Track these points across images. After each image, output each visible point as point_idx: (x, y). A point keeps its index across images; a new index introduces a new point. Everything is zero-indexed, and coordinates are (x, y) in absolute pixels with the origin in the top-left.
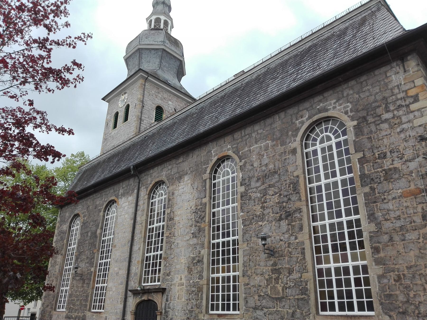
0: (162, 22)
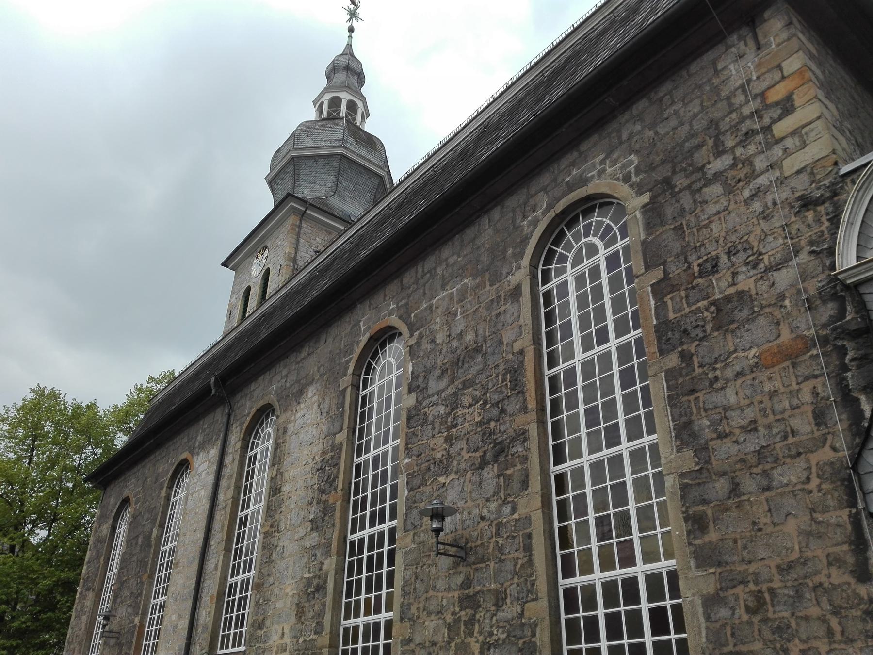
0: (344, 104)
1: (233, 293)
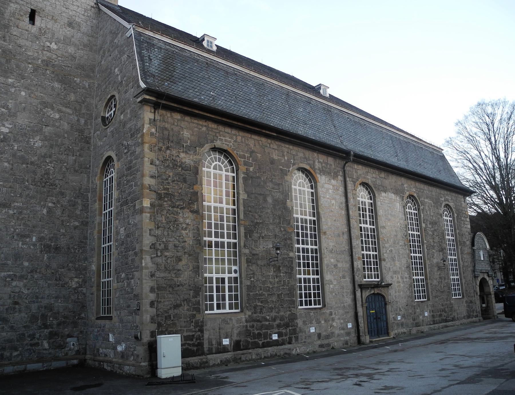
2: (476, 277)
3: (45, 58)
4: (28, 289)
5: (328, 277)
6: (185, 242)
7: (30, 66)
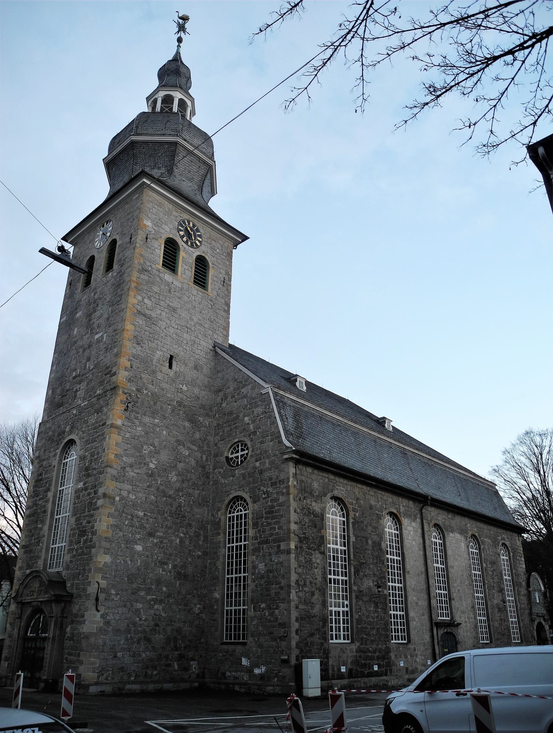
0: (176, 102)
1: (226, 283)
2: (532, 621)
3: (179, 399)
4: (165, 613)
5: (412, 614)
6: (316, 579)
7: (170, 407)
